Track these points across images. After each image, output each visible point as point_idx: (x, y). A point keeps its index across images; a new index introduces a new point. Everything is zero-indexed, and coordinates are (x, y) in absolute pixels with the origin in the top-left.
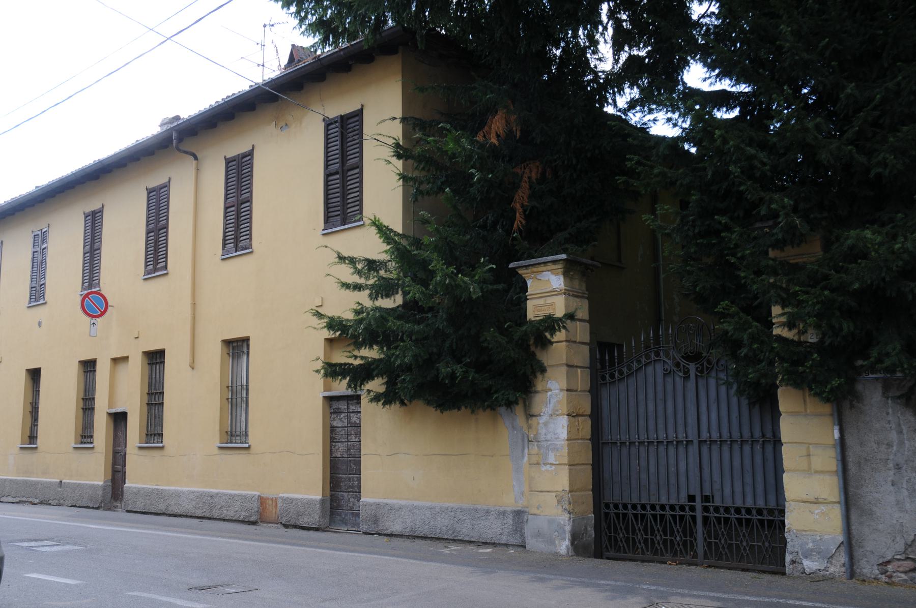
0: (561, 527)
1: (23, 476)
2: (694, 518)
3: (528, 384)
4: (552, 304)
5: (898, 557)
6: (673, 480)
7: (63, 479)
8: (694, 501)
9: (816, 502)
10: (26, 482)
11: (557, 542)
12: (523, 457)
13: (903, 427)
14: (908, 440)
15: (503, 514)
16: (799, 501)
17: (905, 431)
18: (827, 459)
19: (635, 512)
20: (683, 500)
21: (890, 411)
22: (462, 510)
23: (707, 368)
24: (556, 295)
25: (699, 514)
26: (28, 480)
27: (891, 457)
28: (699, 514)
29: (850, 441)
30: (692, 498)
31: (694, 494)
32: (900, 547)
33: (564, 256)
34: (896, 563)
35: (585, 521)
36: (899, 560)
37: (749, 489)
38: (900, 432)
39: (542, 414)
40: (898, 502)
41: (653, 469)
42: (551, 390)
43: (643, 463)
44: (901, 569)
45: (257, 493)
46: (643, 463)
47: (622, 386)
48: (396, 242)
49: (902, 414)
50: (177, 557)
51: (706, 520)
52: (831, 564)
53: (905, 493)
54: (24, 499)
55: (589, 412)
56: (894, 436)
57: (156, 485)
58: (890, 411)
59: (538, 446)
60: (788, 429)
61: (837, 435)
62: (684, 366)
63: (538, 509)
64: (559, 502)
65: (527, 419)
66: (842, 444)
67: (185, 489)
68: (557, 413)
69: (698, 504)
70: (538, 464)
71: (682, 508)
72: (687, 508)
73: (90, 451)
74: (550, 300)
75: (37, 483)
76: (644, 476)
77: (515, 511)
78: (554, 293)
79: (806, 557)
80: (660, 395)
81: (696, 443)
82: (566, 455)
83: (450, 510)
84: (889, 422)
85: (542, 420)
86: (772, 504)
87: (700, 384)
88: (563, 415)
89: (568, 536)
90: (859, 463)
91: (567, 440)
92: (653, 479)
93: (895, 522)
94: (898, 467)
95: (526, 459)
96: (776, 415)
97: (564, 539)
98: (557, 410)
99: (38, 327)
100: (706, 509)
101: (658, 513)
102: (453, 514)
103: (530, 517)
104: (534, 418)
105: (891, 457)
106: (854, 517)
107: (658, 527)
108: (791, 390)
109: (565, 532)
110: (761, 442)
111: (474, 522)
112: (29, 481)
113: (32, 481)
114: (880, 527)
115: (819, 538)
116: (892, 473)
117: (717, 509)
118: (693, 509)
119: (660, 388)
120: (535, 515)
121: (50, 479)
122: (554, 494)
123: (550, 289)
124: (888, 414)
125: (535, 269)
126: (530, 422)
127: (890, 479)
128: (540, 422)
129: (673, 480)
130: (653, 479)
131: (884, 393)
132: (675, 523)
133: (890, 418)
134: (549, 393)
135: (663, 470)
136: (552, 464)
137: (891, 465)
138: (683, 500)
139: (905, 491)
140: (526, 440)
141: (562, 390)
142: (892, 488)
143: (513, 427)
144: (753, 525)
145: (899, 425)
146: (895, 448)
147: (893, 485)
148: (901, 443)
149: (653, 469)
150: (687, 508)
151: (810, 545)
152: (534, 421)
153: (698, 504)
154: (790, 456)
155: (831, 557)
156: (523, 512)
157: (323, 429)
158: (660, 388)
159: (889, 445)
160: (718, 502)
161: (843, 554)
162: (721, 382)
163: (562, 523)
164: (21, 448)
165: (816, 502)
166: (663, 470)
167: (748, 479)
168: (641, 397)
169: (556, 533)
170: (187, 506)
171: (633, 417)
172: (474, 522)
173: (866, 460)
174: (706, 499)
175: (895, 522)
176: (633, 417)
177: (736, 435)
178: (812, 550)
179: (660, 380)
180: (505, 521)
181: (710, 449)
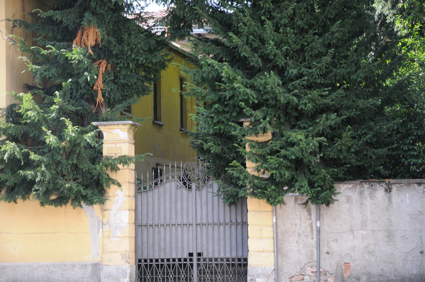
0: (124, 273)
2: (192, 265)
3: (104, 192)
4: (120, 148)
5: (297, 274)
6: (180, 245)
8: (193, 256)
9: (263, 251)
11: (121, 279)
12: (98, 233)
13: (302, 217)
14: (304, 223)
15: (85, 266)
16: (255, 252)
17: (303, 219)
18: (269, 232)
19: (157, 263)
20: (186, 256)
21: (297, 210)
22: (54, 265)
23: (202, 186)
24: (123, 143)
25: (195, 262)
27: (296, 230)
28: (195, 262)
29: (279, 223)
30: (191, 255)
31: (192, 252)
32: (298, 269)
33: (131, 122)
34: (296, 277)
36: (297, 275)
37: (222, 249)
38: (301, 219)
39: (112, 209)
40: (298, 250)
41: (168, 239)
42: (118, 196)
43: (162, 236)
44: (298, 279)
46: (162, 236)
47: (150, 194)
48: (38, 111)
49: (302, 211)
51: (198, 265)
52: (269, 279)
53: (301, 246)
55: (134, 209)
56: (298, 221)
58: (297, 210)
59: (109, 227)
60: (251, 218)
61: (274, 221)
62: (189, 185)
63: (109, 262)
64: (123, 258)
65: (102, 212)
66: (276, 226)
68: (122, 208)
69: (195, 258)
70: (109, 237)
71: (185, 260)
72: (188, 260)
74: (118, 145)
76: (162, 244)
77: (93, 264)
78: (122, 141)
79: (258, 277)
80: (173, 200)
81: (194, 225)
83: (45, 266)
84: (296, 215)
85: (112, 213)
86: (240, 255)
87: (197, 194)
88: (126, 209)
89: (128, 276)
90: (283, 233)
91: (129, 223)
92: (168, 244)
93: (296, 259)
94: (299, 235)
95: (101, 234)
96: (244, 212)
97: (126, 277)
98: (122, 207)
100: (199, 260)
101: (182, 263)
102: (47, 268)
103: (104, 267)
104: (107, 211)
105: (296, 230)
106: (279, 258)
107: (171, 271)
109: (126, 273)
110: (230, 225)
111: (63, 272)
114: (290, 261)
115: (264, 268)
116: (296, 237)
117: (205, 260)
118: (191, 260)
119: (173, 196)
120: (107, 265)
122: (120, 253)
123: (119, 139)
124: (296, 211)
125: (110, 127)
126: (104, 213)
127: (296, 240)
128: (111, 213)
129: (180, 245)
130: (168, 244)
131: (295, 202)
132: (181, 268)
133: (297, 213)
134: (117, 197)
135: (174, 240)
136: (118, 237)
137: (296, 234)
138: (186, 256)
139: (301, 245)
140: (101, 223)
141: (125, 196)
142: (296, 244)
143: (92, 216)
144: (224, 267)
145: (301, 216)
146: (298, 226)
147: (297, 243)
148: (301, 224)
149: (168, 239)
150: (188, 260)
151: (260, 272)
152: (106, 213)
153: (195, 258)
154: (252, 230)
155: (269, 276)
156: (99, 264)
158: (173, 196)
159: (296, 225)
160: (205, 256)
161: (274, 274)
162: (215, 195)
163: (125, 268)
165: (263, 251)
166: (174, 240)
167: (222, 243)
168: (162, 200)
169: (121, 274)
171: (156, 211)
172: (63, 272)
173: (286, 232)
174: (199, 254)
175: (296, 259)
176: (156, 211)
177: (222, 221)
178: (260, 274)
179: (173, 191)
180: (86, 270)
181: (213, 229)
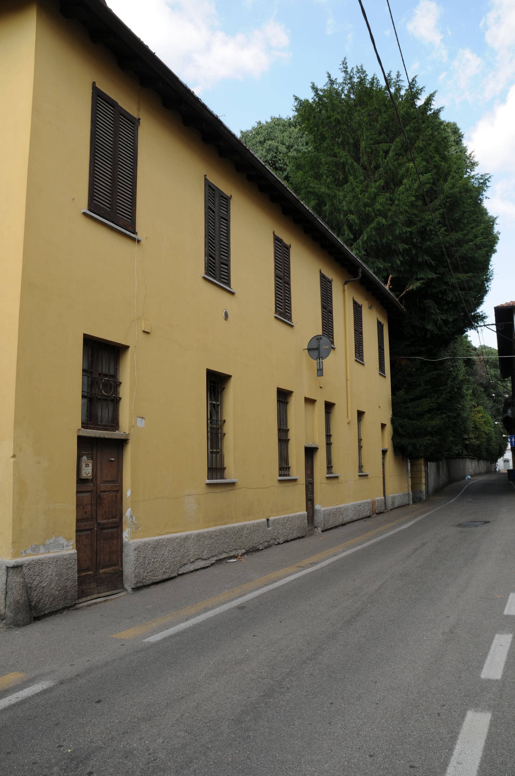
1: (216, 525)
7: (270, 517)
10: (225, 533)
26: (227, 528)
35: (431, 404)
45: (369, 500)
50: (190, 734)
54: (224, 556)
57: (336, 505)
67: (349, 504)
73: (293, 484)
75: (243, 528)
82: (219, 608)
99: (228, 312)
108: (494, 349)
112: (230, 529)
113: (234, 528)
121: (254, 520)
157: (16, 403)
164: (208, 485)
170: (350, 516)
